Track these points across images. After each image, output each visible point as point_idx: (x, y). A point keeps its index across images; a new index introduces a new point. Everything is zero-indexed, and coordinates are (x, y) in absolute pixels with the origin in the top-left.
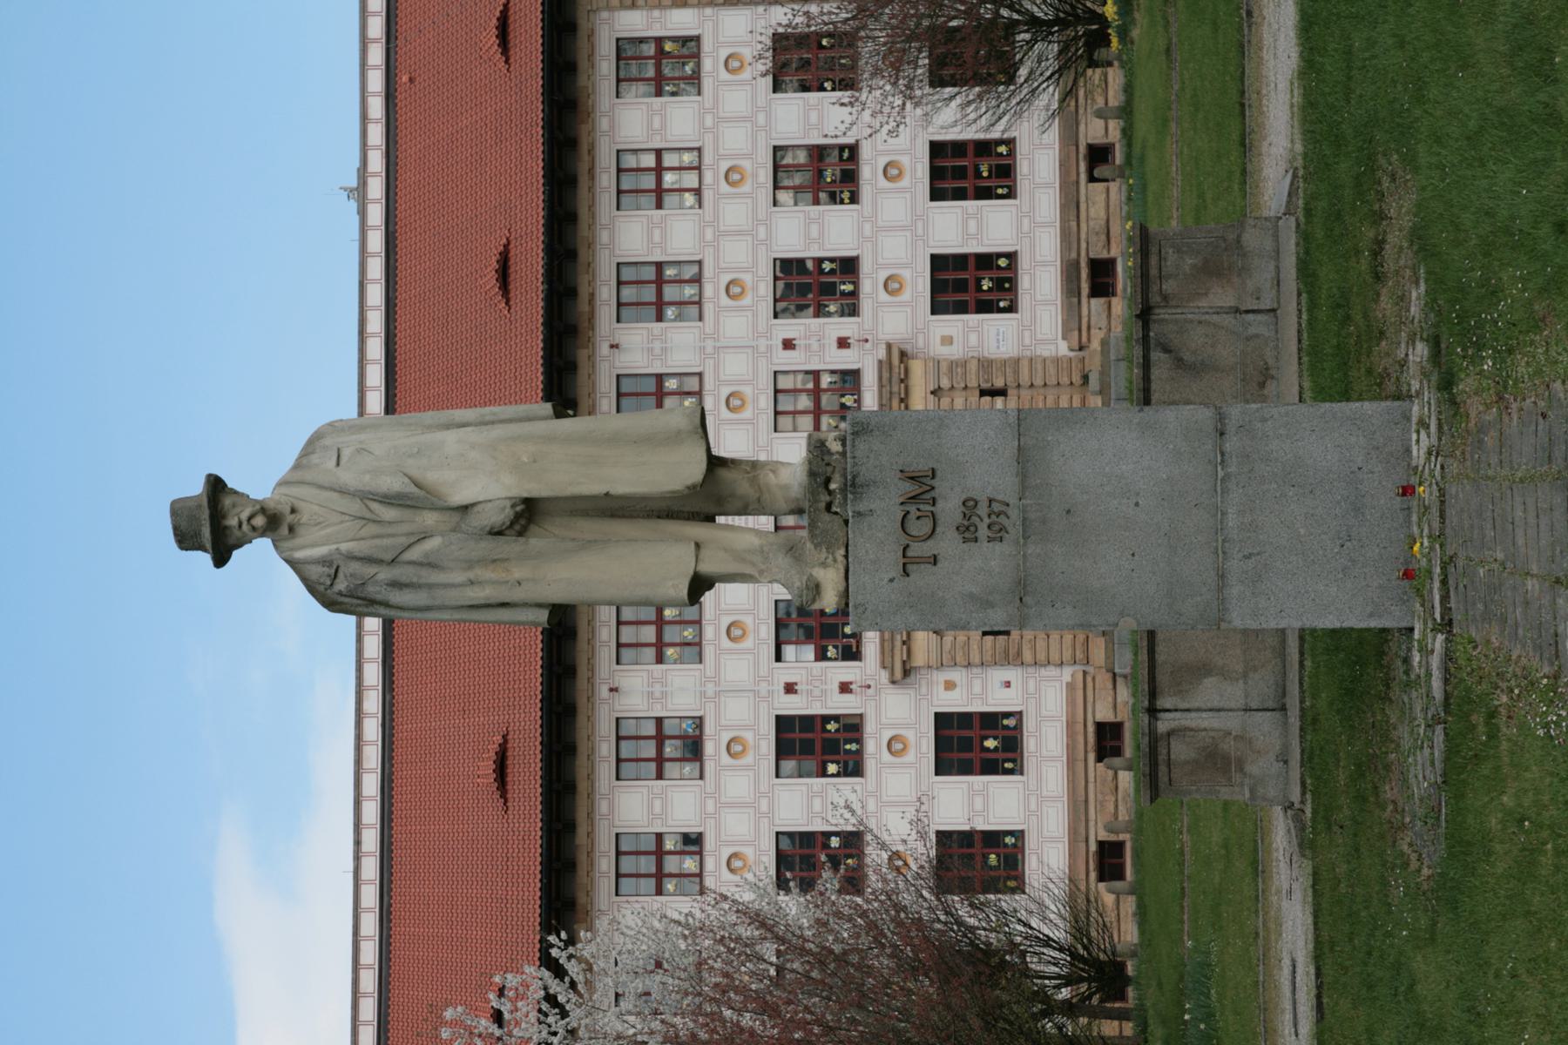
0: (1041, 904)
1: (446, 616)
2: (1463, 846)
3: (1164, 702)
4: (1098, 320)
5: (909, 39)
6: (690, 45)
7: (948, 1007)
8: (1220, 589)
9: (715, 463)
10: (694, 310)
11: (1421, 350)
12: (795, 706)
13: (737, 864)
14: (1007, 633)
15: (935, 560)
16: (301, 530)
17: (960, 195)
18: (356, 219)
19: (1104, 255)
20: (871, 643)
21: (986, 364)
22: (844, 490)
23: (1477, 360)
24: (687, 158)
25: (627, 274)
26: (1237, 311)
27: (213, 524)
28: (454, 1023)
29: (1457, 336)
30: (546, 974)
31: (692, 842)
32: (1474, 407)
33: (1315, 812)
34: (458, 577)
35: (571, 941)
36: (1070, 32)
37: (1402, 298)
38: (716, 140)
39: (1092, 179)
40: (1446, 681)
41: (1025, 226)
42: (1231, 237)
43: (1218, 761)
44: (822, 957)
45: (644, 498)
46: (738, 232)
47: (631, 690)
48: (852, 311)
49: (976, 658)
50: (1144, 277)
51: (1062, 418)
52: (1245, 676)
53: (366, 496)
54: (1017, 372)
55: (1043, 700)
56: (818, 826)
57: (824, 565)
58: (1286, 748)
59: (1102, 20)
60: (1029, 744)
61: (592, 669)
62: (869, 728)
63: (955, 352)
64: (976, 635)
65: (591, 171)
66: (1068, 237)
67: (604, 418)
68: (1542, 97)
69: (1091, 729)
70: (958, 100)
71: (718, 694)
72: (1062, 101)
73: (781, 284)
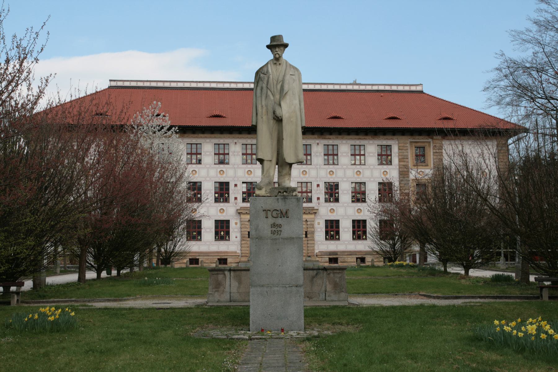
0: (184, 245)
1: (254, 100)
2: (198, 342)
3: (232, 273)
4: (323, 260)
5: (391, 215)
6: (390, 163)
7: (160, 223)
8: (259, 286)
9: (290, 165)
10: (327, 163)
11: (316, 334)
12: (231, 187)
13: (194, 172)
14: (249, 237)
15: (267, 217)
16: (275, 66)
17: (354, 227)
18: (349, 83)
19: (339, 261)
20: (247, 205)
21: (313, 233)
22: (284, 196)
23: (314, 346)
24: (363, 162)
25: (335, 147)
26: (326, 291)
27: (277, 45)
28: (157, 104)
29: (320, 342)
30: (168, 126)
31: (199, 162)
32: (303, 345)
33: (206, 308)
34: (264, 103)
35: (176, 133)
36: (392, 253)
37: (328, 329)
38: (367, 169)
39: (357, 258)
40: (237, 339)
41: (346, 242)
42: (343, 290)
43: (218, 286)
44: (172, 192)
45: (282, 148)
46: (345, 174)
47: (236, 147)
48: (326, 201)
49: (243, 230)
50: (334, 269)
51: (301, 249)
52: (238, 292)
53: (283, 81)
54: (311, 240)
55: (233, 246)
56: (203, 192)
57: (266, 191)
58: (221, 302)
59: (395, 261)
60: (222, 243)
61: (241, 138)
62: (226, 204)
63: (316, 225)
64: (249, 230)
65: (360, 139)
66: (343, 253)
67: (302, 141)
68: (377, 361)
69: (226, 257)
70: (376, 227)
71: (235, 168)
72: (376, 251)
73: (332, 184)
